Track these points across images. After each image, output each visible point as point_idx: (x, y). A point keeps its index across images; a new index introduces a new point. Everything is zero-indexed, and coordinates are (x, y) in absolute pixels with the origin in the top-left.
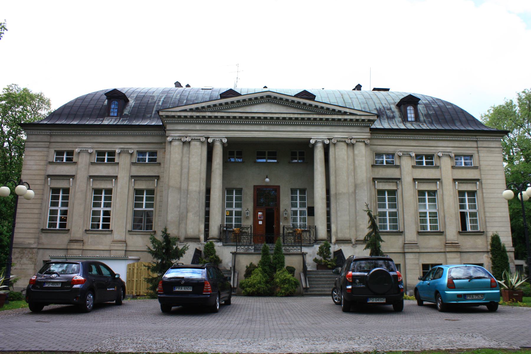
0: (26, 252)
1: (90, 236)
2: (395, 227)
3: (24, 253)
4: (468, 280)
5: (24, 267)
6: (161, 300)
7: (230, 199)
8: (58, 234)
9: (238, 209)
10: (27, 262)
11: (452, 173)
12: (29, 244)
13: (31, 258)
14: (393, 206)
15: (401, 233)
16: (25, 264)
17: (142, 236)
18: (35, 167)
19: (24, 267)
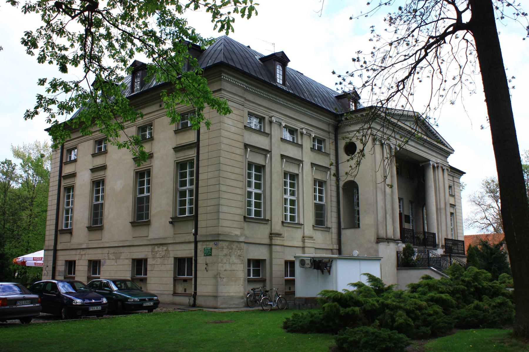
0: (234, 246)
1: (286, 228)
2: (292, 218)
3: (232, 249)
4: (355, 288)
5: (234, 267)
6: (25, 266)
7: (183, 175)
8: (259, 225)
9: (258, 191)
10: (236, 261)
11: (302, 157)
12: (236, 235)
13: (239, 256)
14: (293, 193)
15: (266, 221)
16: (234, 264)
17: (322, 232)
18: (233, 129)
19: (234, 267)
